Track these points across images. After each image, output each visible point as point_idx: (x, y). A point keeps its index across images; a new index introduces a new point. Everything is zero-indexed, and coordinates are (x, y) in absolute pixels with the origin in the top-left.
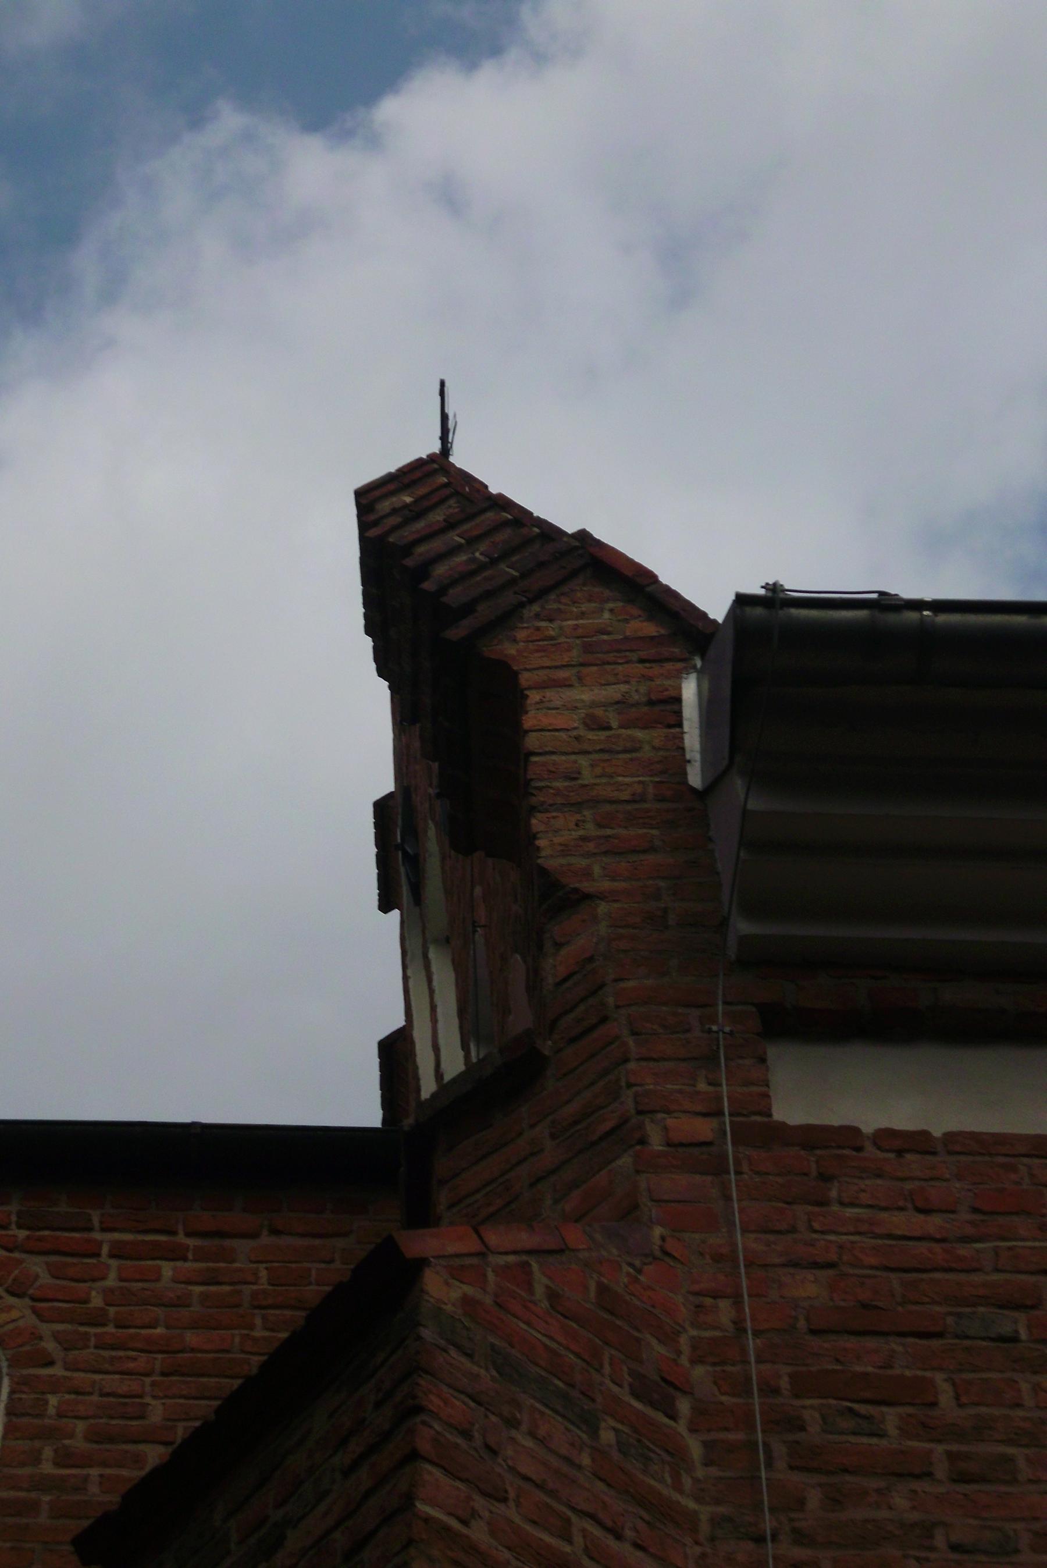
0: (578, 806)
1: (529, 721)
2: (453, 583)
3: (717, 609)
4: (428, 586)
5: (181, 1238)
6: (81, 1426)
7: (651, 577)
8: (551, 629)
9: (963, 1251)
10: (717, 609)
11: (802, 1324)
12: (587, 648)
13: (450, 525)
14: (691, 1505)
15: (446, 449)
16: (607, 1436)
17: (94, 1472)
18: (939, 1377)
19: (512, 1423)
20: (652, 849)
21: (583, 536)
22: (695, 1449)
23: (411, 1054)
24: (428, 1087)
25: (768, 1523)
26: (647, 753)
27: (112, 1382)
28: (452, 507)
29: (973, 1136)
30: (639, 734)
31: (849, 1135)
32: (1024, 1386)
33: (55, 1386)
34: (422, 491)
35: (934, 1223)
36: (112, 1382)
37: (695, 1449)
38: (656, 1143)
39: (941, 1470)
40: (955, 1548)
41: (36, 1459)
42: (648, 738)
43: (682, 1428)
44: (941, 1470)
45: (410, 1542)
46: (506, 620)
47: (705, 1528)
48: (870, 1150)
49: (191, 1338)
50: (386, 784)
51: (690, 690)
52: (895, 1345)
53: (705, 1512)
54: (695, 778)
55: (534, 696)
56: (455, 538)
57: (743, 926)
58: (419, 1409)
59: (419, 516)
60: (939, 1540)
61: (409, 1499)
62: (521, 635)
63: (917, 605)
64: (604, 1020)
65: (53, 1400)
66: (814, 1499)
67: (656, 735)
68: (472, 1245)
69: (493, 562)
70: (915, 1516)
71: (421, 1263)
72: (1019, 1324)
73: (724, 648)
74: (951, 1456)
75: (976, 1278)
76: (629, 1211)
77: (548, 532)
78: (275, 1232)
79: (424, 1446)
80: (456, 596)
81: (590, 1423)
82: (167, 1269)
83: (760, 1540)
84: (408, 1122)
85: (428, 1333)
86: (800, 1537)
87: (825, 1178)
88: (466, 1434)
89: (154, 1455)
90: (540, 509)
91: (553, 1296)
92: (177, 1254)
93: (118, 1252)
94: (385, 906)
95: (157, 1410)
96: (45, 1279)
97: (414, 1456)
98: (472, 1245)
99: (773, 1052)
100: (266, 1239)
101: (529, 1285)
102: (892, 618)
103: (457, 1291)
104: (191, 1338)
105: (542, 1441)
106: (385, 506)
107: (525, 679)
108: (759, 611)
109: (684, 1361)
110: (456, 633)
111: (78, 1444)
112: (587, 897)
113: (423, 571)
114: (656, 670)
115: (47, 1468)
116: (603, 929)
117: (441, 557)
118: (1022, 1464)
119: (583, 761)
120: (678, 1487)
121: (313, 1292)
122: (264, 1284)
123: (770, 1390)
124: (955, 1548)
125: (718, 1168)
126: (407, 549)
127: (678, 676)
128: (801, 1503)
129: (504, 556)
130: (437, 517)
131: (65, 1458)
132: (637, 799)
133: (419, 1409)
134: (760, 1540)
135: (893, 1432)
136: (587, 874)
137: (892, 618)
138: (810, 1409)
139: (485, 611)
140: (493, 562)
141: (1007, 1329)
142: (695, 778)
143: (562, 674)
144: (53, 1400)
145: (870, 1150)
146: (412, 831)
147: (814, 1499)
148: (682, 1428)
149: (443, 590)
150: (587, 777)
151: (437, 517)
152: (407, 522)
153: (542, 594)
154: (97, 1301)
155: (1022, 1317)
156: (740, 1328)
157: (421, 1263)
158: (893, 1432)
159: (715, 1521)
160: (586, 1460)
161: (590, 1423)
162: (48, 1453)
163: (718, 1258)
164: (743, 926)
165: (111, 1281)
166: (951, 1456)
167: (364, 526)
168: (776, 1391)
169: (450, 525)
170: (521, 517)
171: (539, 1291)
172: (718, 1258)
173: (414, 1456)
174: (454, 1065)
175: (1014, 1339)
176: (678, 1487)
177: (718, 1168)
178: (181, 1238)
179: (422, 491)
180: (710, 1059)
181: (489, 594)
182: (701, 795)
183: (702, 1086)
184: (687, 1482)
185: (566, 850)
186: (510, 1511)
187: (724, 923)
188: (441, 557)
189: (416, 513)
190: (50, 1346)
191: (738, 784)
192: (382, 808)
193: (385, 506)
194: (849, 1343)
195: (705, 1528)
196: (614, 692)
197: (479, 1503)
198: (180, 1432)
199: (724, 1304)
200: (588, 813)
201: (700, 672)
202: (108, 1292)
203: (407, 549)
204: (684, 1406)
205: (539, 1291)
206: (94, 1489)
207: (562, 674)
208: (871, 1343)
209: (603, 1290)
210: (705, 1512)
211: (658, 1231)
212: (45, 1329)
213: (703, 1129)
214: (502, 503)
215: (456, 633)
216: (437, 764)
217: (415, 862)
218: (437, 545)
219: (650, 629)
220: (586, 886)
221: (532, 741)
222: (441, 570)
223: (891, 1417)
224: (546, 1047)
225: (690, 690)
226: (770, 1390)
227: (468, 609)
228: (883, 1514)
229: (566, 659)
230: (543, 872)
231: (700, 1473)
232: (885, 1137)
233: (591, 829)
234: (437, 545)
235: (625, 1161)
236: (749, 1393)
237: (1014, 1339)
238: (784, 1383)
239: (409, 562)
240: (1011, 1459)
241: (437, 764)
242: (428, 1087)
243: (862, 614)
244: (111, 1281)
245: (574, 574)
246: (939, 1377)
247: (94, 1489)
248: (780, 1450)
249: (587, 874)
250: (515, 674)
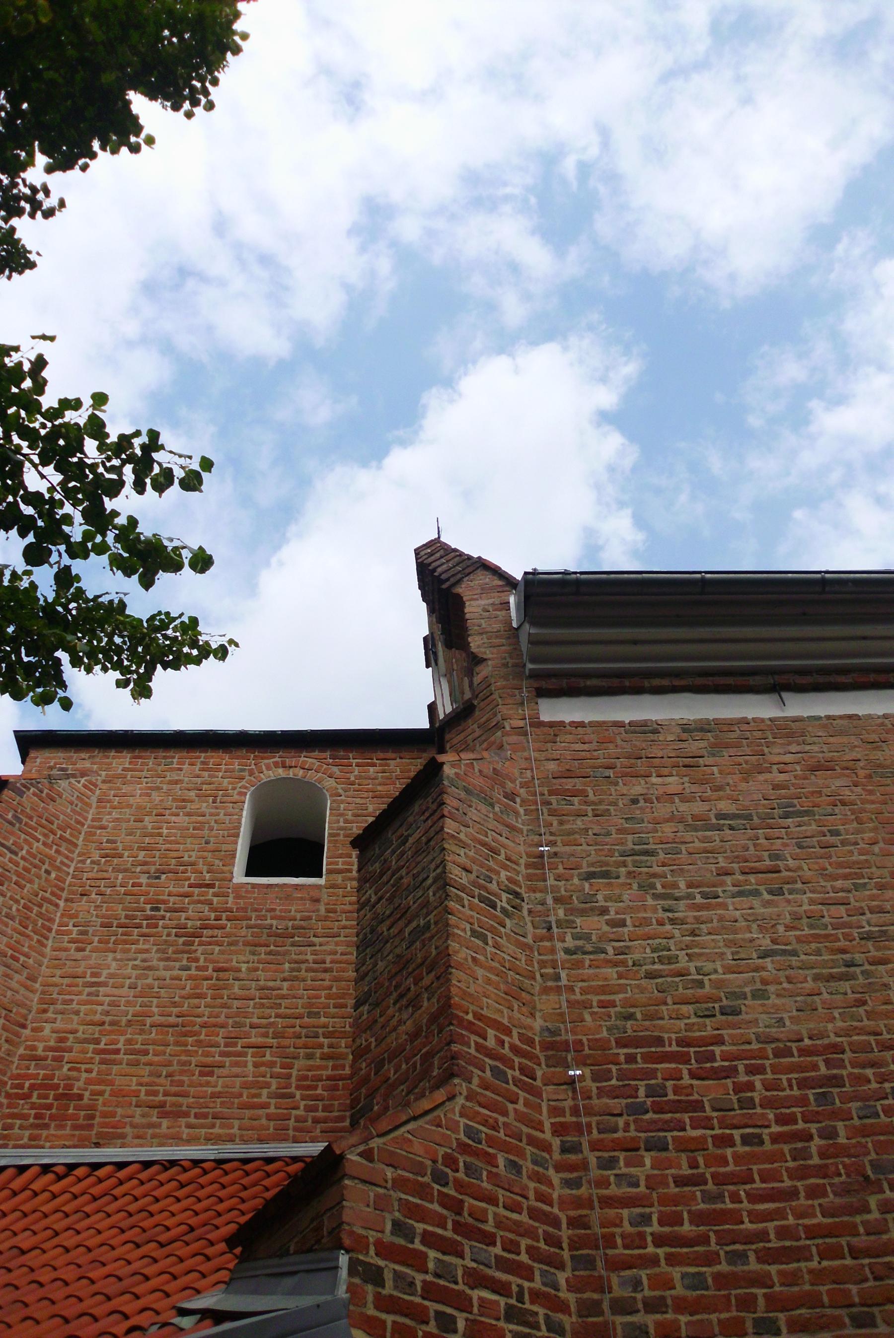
0: (482, 634)
1: (466, 611)
2: (443, 573)
3: (519, 576)
4: (436, 574)
5: (375, 761)
6: (350, 813)
7: (500, 568)
8: (472, 584)
9: (595, 753)
10: (519, 576)
11: (550, 776)
12: (482, 589)
13: (442, 557)
14: (522, 827)
15: (439, 537)
16: (497, 809)
17: (355, 825)
18: (589, 789)
19: (470, 806)
20: (503, 645)
21: (479, 558)
22: (522, 811)
23: (436, 708)
24: (442, 716)
25: (543, 830)
26: (501, 618)
27: (358, 800)
28: (442, 552)
29: (597, 722)
30: (499, 613)
31: (561, 724)
32: (613, 790)
33: (342, 802)
34: (433, 548)
35: (586, 747)
36: (358, 800)
37: (522, 811)
38: (508, 728)
39: (590, 814)
40: (595, 834)
41: (338, 822)
42: (501, 614)
43: (518, 806)
44: (590, 814)
45: (443, 839)
46: (459, 581)
47: (525, 832)
48: (568, 727)
49: (379, 788)
50: (426, 632)
51: (512, 600)
52: (576, 780)
53: (525, 828)
54: (515, 625)
55: (467, 604)
56: (443, 560)
57: (530, 666)
58: (444, 803)
59: (432, 555)
60: (590, 833)
61: (442, 828)
62: (463, 586)
63: (575, 573)
64: (491, 694)
65: (342, 806)
66: (555, 823)
67: (503, 613)
68: (457, 758)
69: (454, 566)
70: (583, 827)
71: (443, 763)
72: (611, 773)
73: (521, 587)
74: (593, 810)
75: (599, 761)
76: (501, 747)
77: (469, 558)
78: (401, 758)
79: (446, 813)
80: (443, 577)
81: (492, 805)
82: (372, 769)
83: (541, 835)
84: (437, 725)
85: (446, 783)
86: (552, 834)
87: (555, 735)
88: (458, 810)
89: (371, 819)
90: (466, 551)
91: (480, 771)
92: (374, 765)
93: (358, 765)
94: (428, 666)
95: (371, 808)
96: (338, 773)
97: (443, 816)
98: (457, 758)
99: (540, 701)
100: (398, 760)
101: (474, 769)
102: (568, 577)
103: (453, 771)
104: (379, 788)
105: (479, 811)
106: (422, 553)
107: (465, 599)
108: (531, 576)
109: (518, 787)
110: (444, 586)
111: (350, 817)
112: (486, 660)
113: (434, 570)
114: (502, 594)
115: (342, 824)
116: (490, 668)
117: (439, 566)
118: (612, 811)
119: (483, 621)
120: (517, 822)
121: (412, 774)
122: (398, 773)
123: (542, 794)
124: (595, 834)
125: (526, 734)
126: (430, 564)
127: (508, 596)
128: (552, 825)
129: (457, 564)
130: (438, 555)
131: (346, 821)
132: (498, 631)
133: (444, 803)
134: (541, 835)
135: (577, 804)
136: (485, 653)
137: (568, 577)
138: (553, 799)
139: (452, 580)
140: (454, 566)
141: (607, 775)
142: (515, 625)
143: (476, 597)
144: (342, 806)
145: (568, 727)
146: (434, 645)
147: (555, 823)
148: (518, 806)
149: (440, 575)
150: (484, 626)
151: (438, 555)
152: (429, 557)
153: (469, 574)
154: (352, 779)
155: (611, 771)
156: (533, 778)
157: (443, 763)
158: (577, 804)
159: (528, 831)
160: (491, 815)
161: (492, 805)
162: (342, 820)
163: (526, 759)
164: (530, 666)
165: (356, 773)
166: (593, 810)
167: (417, 559)
168: (544, 795)
169: (442, 557)
170: (461, 554)
171: (476, 770)
172: (526, 759)
173: (443, 816)
174: (449, 709)
175: (609, 777)
176: (517, 822)
177: (526, 734)
178: (375, 761)
179: (433, 548)
180: (522, 704)
181: (453, 575)
182: (517, 629)
183: (520, 711)
184: (520, 820)
185: (479, 647)
186: (470, 830)
187: (525, 665)
188: (439, 566)
189: (431, 554)
190: (340, 791)
191: (527, 626)
192: (425, 639)
193: (422, 553)
194: (564, 780)
195: (525, 832)
196: (491, 601)
197: (462, 828)
198: (378, 813)
199: (528, 771)
200: (484, 636)
201: (515, 595)
202: (355, 776)
203: (430, 564)
204: (518, 800)
205: (476, 770)
206: (355, 829)
207: (476, 597)
208: (570, 780)
209: (494, 769)
210: (525, 828)
211: (509, 752)
212: (339, 786)
213: (521, 723)
214: (455, 550)
215: (444, 586)
216: (106, 639)
217: (435, 654)
218: (438, 563)
219: (500, 583)
220: (485, 657)
221: (467, 616)
222: (439, 570)
223: (576, 800)
224: (475, 702)
225: (512, 600)
226: (542, 794)
227: (448, 579)
228: (574, 826)
229: (476, 592)
230: (472, 653)
231: (523, 818)
232: (572, 724)
233: (486, 640)
234: (438, 563)
235: (499, 733)
236: (536, 795)
237: (609, 777)
238: (546, 792)
239: (430, 568)
240: (608, 810)
241: (106, 639)
242: (442, 716)
243: (560, 576)
244: (356, 773)
245: (478, 568)
246: (589, 789)
247: (355, 829)
248: (545, 811)
249: (485, 653)
250: (462, 598)
